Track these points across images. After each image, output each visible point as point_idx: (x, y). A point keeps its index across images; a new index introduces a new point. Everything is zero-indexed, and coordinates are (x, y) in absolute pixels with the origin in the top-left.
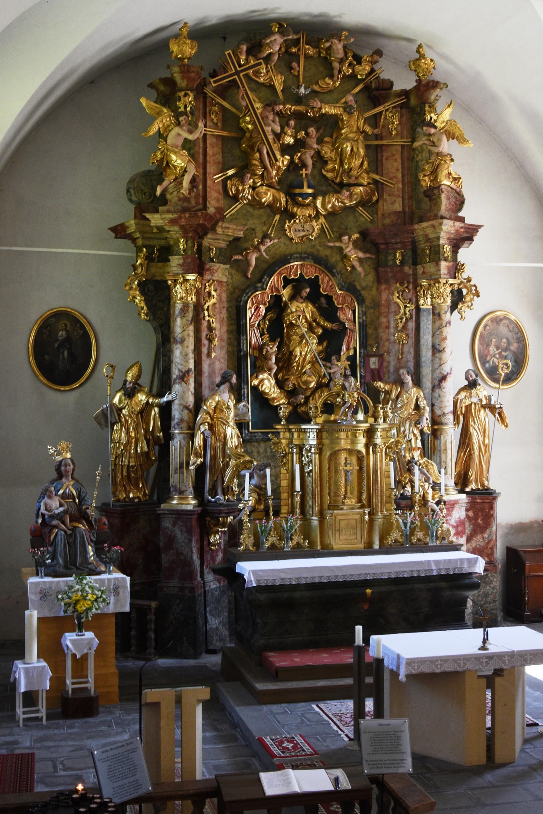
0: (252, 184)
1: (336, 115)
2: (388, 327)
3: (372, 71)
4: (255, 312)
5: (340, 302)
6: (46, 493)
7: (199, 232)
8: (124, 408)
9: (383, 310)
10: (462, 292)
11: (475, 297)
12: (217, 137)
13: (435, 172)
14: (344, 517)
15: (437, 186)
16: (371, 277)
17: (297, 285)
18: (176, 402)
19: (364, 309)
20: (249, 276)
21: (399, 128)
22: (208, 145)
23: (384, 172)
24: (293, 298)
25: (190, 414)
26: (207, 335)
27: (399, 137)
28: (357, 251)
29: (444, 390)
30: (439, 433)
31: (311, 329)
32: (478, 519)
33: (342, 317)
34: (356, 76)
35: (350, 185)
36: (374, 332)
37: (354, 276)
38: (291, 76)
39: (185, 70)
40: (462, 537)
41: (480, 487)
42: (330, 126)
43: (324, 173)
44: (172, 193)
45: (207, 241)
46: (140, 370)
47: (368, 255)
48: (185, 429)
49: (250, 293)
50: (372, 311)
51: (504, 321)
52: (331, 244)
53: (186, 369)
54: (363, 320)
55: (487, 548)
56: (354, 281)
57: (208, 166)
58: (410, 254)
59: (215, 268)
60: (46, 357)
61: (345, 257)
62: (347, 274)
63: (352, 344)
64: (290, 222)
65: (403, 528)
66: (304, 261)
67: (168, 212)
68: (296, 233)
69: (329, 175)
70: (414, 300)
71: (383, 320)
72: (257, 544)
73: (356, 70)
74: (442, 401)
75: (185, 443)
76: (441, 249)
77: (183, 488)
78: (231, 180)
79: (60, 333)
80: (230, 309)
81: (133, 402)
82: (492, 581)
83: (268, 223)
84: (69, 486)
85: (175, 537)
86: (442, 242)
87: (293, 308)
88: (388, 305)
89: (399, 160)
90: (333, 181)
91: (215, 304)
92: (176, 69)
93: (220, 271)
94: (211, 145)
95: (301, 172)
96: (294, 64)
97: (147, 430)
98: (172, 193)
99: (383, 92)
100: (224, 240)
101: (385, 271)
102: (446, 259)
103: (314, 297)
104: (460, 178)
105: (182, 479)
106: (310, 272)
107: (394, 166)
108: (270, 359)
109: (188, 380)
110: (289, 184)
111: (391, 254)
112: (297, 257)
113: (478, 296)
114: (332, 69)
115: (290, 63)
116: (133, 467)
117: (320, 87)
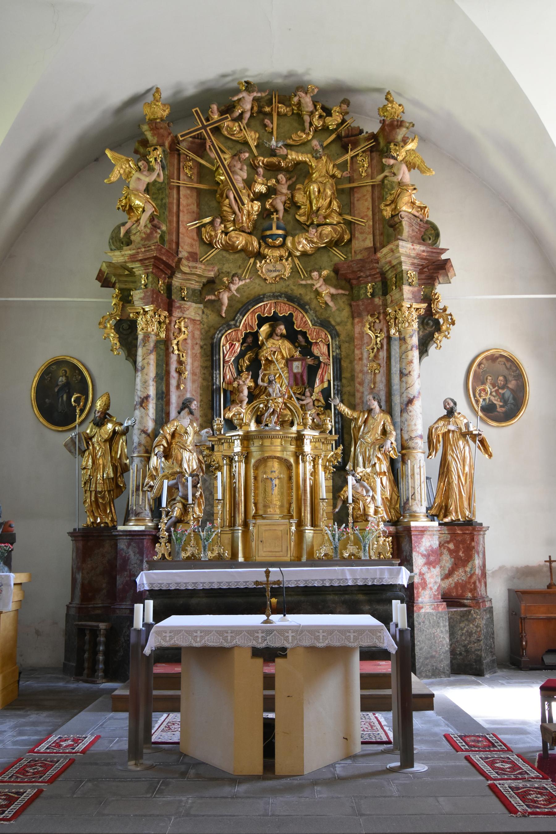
0: (223, 229)
2: (361, 359)
3: (343, 121)
4: (230, 349)
5: (314, 337)
8: (93, 437)
9: (357, 342)
10: (439, 322)
11: (451, 325)
12: (192, 189)
13: (394, 201)
14: (268, 528)
15: (397, 213)
16: (346, 313)
17: (274, 320)
18: (136, 427)
19: (337, 343)
20: (224, 315)
21: (369, 170)
22: (181, 196)
23: (356, 212)
25: (148, 438)
26: (176, 369)
27: (370, 178)
28: (328, 286)
29: (410, 414)
30: (406, 458)
32: (459, 552)
34: (328, 127)
35: (319, 225)
36: (349, 365)
37: (329, 312)
38: (266, 134)
40: (434, 567)
41: (460, 517)
42: (300, 173)
43: (297, 217)
44: (135, 234)
45: (177, 281)
47: (341, 291)
48: (142, 452)
49: (224, 331)
50: (347, 345)
51: (500, 359)
52: (304, 282)
53: (145, 395)
54: (337, 354)
55: (470, 582)
56: (329, 317)
57: (181, 214)
58: (380, 285)
59: (186, 306)
60: (47, 400)
61: (318, 293)
62: (321, 311)
63: (326, 376)
64: (261, 262)
65: (331, 538)
66: (278, 299)
68: (269, 273)
69: (302, 219)
70: (385, 329)
71: (357, 352)
73: (326, 122)
74: (408, 425)
75: (141, 465)
76: (405, 275)
77: (139, 510)
78: (205, 227)
79: (60, 379)
80: (205, 347)
81: (102, 431)
82: (475, 618)
85: (129, 559)
86: (404, 267)
87: (269, 344)
88: (362, 338)
89: (370, 200)
90: (305, 224)
91: (185, 339)
93: (191, 309)
94: (185, 196)
95: (272, 216)
96: (266, 120)
98: (135, 234)
99: (353, 138)
100: (197, 282)
101: (358, 305)
102: (410, 284)
103: (292, 336)
104: (426, 207)
106: (284, 310)
107: (364, 205)
108: (242, 392)
109: (147, 406)
110: (260, 228)
111: (362, 288)
112: (270, 296)
113: (453, 323)
115: (263, 120)
116: (100, 492)
117: (294, 140)
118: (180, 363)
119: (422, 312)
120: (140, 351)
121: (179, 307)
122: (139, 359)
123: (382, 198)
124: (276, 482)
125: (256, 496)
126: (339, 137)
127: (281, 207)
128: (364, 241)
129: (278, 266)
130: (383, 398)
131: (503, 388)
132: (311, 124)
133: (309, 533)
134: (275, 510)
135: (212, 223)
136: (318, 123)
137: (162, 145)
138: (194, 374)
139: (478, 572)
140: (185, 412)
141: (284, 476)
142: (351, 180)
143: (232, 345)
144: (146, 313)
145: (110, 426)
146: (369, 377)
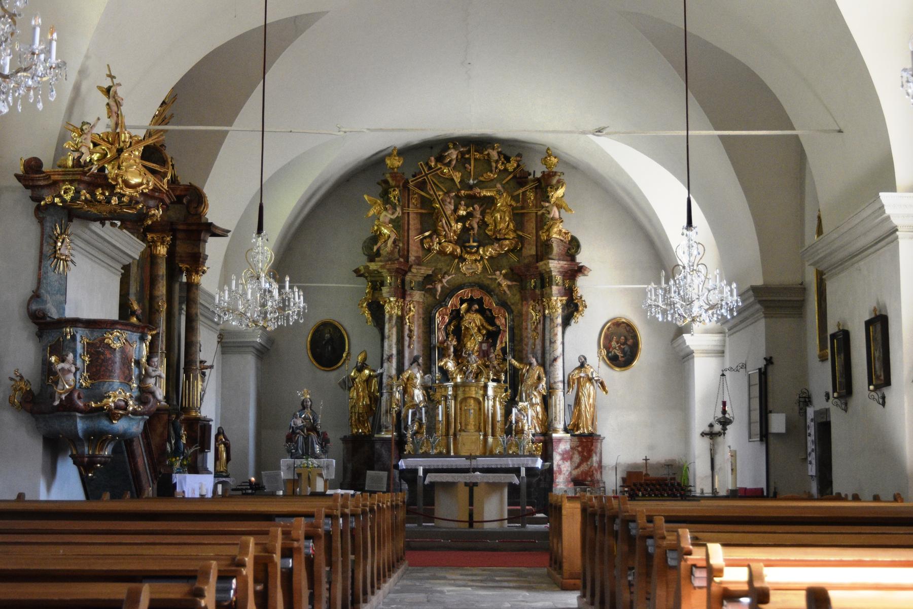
1: (491, 197)
3: (518, 166)
4: (440, 319)
6: (295, 416)
7: (401, 273)
12: (417, 213)
13: (548, 230)
16: (518, 297)
17: (471, 301)
24: (468, 310)
31: (479, 330)
33: (498, 322)
35: (500, 240)
39: (394, 176)
42: (491, 201)
45: (408, 277)
46: (366, 355)
58: (539, 282)
61: (499, 284)
67: (381, 261)
69: (489, 233)
71: (524, 324)
72: (415, 450)
83: (450, 265)
84: (307, 413)
87: (467, 317)
88: (527, 315)
92: (388, 175)
97: (370, 392)
102: (557, 285)
103: (481, 311)
105: (388, 420)
106: (477, 295)
110: (462, 240)
113: (586, 307)
114: (491, 166)
118: (410, 331)
119: (564, 302)
120: (387, 326)
121: (410, 294)
122: (386, 331)
123: (542, 228)
124: (472, 411)
125: (461, 418)
126: (514, 177)
127: (476, 226)
128: (530, 250)
129: (474, 266)
130: (539, 355)
131: (623, 344)
132: (496, 168)
133: (490, 439)
134: (471, 427)
135: (430, 236)
136: (501, 167)
137: (398, 187)
138: (419, 337)
139: (595, 465)
140: (415, 365)
141: (477, 408)
142: (523, 208)
143: (443, 318)
144: (390, 302)
145: (367, 372)
146: (531, 341)
